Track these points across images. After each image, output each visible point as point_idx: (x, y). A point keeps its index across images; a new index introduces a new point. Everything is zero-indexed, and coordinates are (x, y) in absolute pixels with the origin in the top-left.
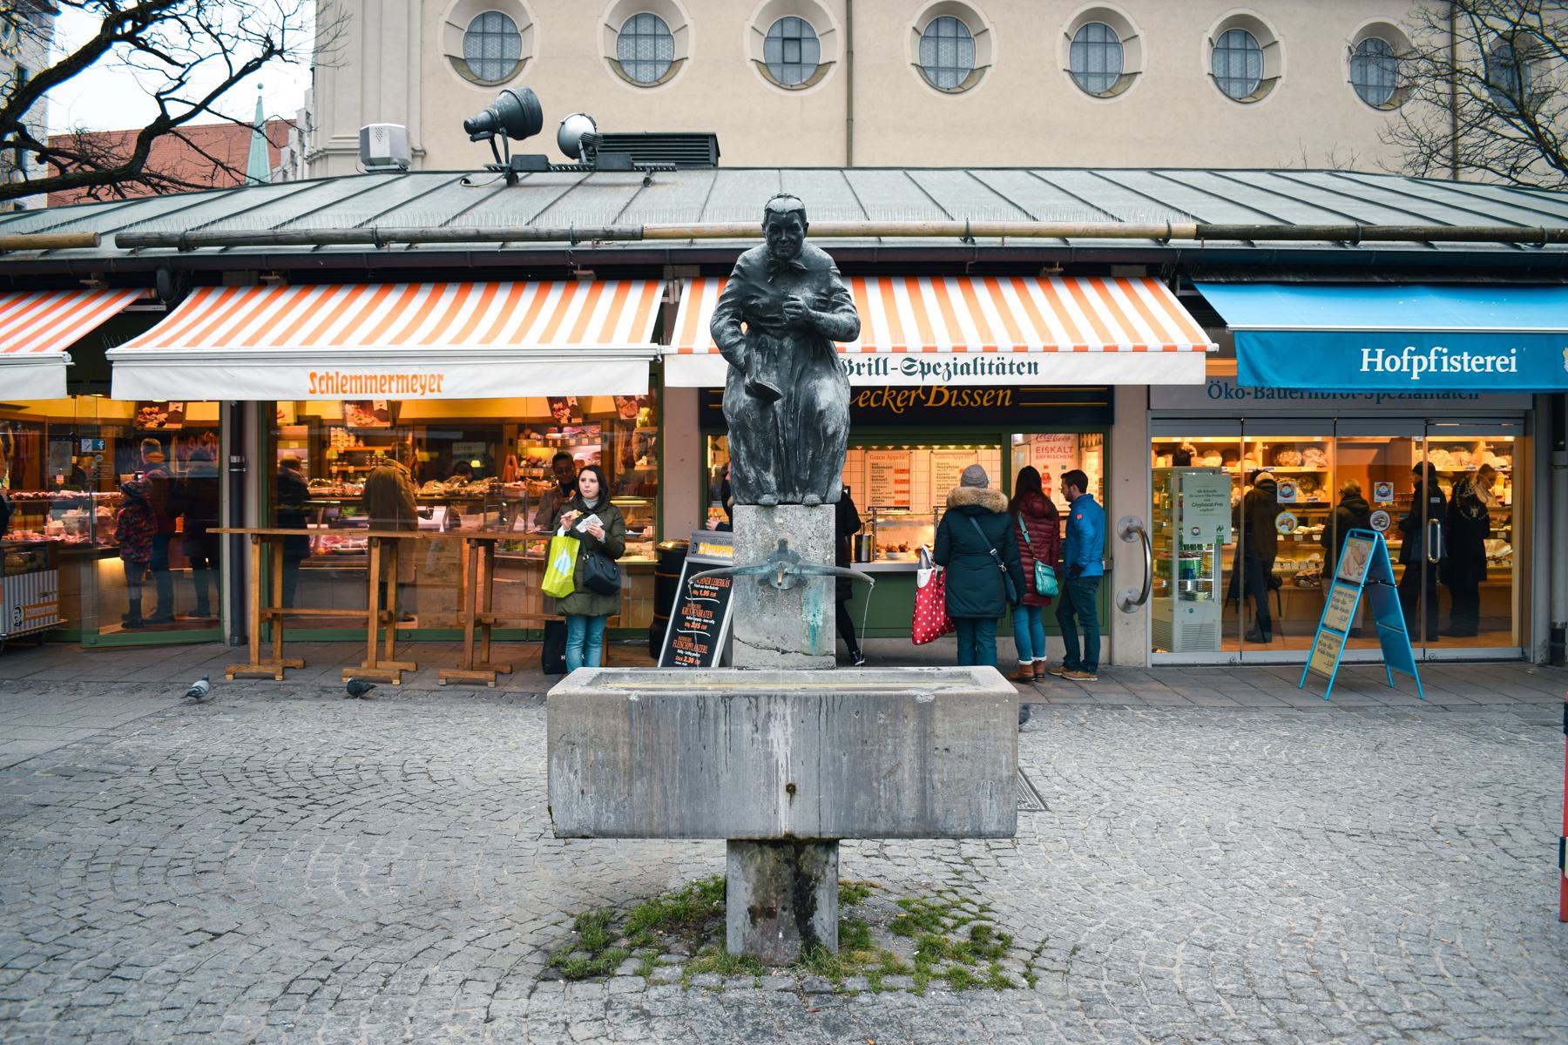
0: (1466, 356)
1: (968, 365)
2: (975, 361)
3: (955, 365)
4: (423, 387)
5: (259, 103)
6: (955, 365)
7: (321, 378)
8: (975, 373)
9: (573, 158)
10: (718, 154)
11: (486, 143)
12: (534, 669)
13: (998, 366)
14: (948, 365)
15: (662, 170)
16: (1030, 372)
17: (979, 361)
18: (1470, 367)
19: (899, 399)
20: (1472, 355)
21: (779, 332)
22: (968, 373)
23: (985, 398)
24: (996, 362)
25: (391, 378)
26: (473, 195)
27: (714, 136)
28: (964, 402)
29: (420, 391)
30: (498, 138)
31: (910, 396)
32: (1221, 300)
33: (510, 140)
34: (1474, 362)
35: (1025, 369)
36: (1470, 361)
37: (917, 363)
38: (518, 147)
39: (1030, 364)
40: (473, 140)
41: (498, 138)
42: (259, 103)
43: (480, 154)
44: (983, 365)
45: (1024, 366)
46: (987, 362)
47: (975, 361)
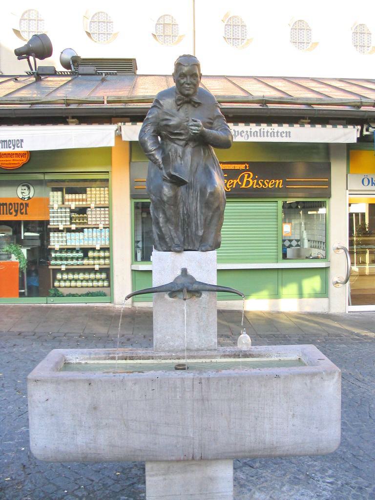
2: (260, 130)
4: (14, 146)
6: (251, 132)
8: (260, 136)
9: (68, 69)
10: (137, 69)
11: (26, 60)
12: (30, 379)
13: (271, 133)
14: (247, 132)
15: (110, 74)
16: (286, 136)
17: (262, 130)
19: (228, 184)
21: (182, 143)
22: (257, 136)
23: (270, 184)
24: (270, 131)
26: (19, 85)
27: (135, 60)
28: (260, 186)
29: (12, 147)
30: (31, 58)
31: (233, 183)
33: (37, 59)
38: (40, 63)
40: (19, 59)
41: (31, 58)
43: (22, 67)
44: (264, 132)
45: (284, 133)
46: (265, 131)
47: (260, 130)
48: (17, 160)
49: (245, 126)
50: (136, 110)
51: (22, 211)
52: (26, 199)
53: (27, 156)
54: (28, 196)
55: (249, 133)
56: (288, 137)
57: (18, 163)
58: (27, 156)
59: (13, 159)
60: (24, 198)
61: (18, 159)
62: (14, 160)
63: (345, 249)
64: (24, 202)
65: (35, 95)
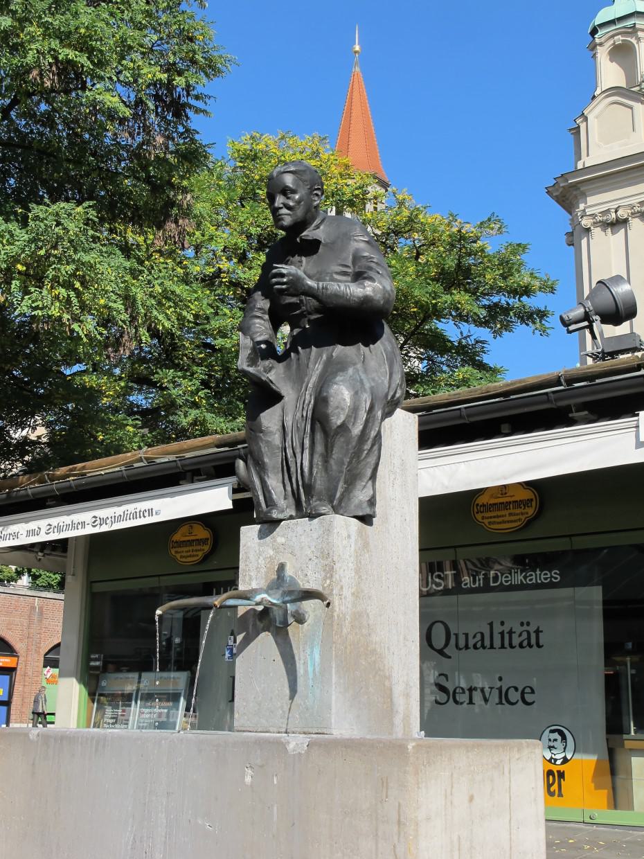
0: (538, 572)
1: (120, 516)
3: (115, 516)
5: (293, 690)
7: (481, 506)
16: (149, 516)
18: (540, 579)
20: (541, 571)
25: (510, 502)
32: (480, 642)
34: (542, 577)
35: (146, 514)
36: (540, 574)
37: (98, 519)
39: (149, 510)
42: (293, 690)
48: (518, 514)
49: (613, 233)
50: (199, 459)
51: (552, 789)
52: (559, 762)
53: (534, 503)
54: (563, 755)
55: (113, 520)
56: (142, 517)
57: (520, 520)
58: (534, 503)
59: (509, 511)
60: (556, 760)
61: (518, 511)
62: (510, 514)
63: (618, 279)
64: (555, 769)
65: (631, 832)
